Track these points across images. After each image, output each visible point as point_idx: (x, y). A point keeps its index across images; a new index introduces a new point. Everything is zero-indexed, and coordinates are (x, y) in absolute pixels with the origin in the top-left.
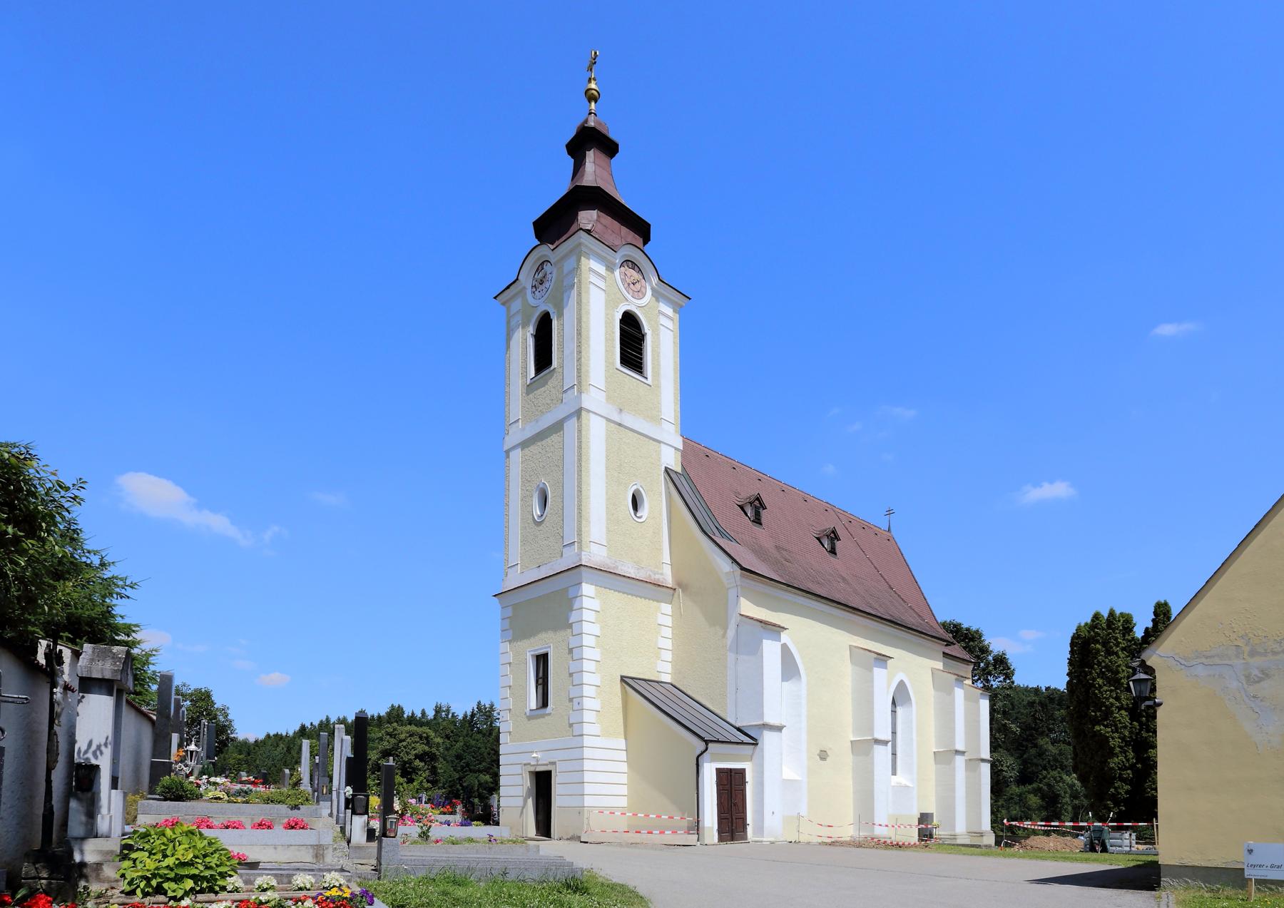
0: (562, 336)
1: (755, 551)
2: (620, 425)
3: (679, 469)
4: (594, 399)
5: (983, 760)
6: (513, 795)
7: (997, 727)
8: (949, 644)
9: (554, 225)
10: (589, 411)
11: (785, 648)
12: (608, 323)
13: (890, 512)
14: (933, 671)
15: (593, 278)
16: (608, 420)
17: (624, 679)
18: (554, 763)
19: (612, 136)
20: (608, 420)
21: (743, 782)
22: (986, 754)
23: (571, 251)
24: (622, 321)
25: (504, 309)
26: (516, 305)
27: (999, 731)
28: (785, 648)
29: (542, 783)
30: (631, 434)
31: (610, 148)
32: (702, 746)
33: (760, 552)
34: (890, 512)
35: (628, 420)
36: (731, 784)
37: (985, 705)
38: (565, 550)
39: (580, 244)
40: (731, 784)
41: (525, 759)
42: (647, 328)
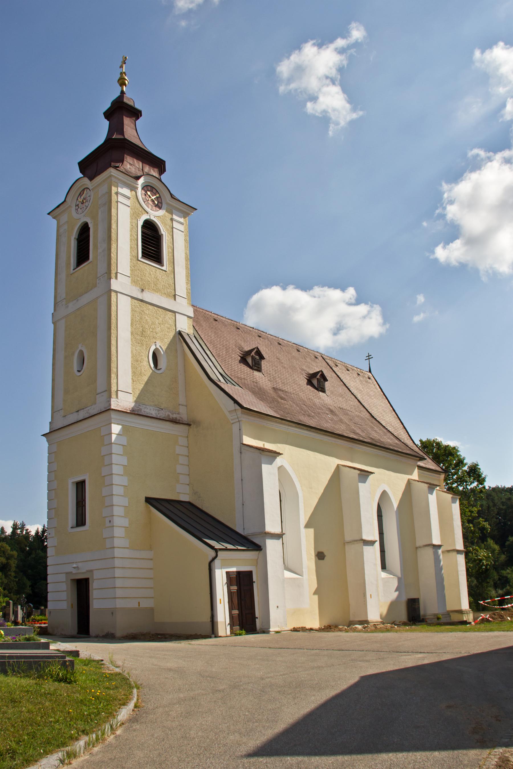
0: (96, 238)
1: (254, 393)
2: (142, 301)
3: (191, 331)
4: (120, 283)
5: (459, 552)
6: (59, 596)
7: (467, 520)
8: (422, 459)
9: (93, 165)
10: (116, 292)
11: (281, 468)
12: (133, 227)
13: (369, 357)
14: (503, 48)
15: (121, 199)
16: (132, 297)
17: (149, 500)
18: (91, 571)
19: (137, 106)
20: (132, 297)
21: (251, 582)
22: (460, 545)
23: (104, 181)
24: (143, 227)
25: (55, 222)
26: (64, 218)
27: (469, 522)
28: (281, 468)
29: (82, 587)
30: (151, 307)
31: (136, 114)
32: (213, 553)
33: (259, 392)
34: (369, 357)
35: (147, 296)
36: (243, 586)
37: (456, 508)
38: (97, 396)
39: (111, 176)
40: (243, 586)
41: (69, 569)
42: (163, 231)
